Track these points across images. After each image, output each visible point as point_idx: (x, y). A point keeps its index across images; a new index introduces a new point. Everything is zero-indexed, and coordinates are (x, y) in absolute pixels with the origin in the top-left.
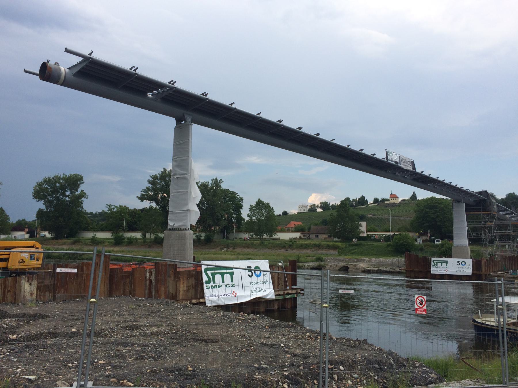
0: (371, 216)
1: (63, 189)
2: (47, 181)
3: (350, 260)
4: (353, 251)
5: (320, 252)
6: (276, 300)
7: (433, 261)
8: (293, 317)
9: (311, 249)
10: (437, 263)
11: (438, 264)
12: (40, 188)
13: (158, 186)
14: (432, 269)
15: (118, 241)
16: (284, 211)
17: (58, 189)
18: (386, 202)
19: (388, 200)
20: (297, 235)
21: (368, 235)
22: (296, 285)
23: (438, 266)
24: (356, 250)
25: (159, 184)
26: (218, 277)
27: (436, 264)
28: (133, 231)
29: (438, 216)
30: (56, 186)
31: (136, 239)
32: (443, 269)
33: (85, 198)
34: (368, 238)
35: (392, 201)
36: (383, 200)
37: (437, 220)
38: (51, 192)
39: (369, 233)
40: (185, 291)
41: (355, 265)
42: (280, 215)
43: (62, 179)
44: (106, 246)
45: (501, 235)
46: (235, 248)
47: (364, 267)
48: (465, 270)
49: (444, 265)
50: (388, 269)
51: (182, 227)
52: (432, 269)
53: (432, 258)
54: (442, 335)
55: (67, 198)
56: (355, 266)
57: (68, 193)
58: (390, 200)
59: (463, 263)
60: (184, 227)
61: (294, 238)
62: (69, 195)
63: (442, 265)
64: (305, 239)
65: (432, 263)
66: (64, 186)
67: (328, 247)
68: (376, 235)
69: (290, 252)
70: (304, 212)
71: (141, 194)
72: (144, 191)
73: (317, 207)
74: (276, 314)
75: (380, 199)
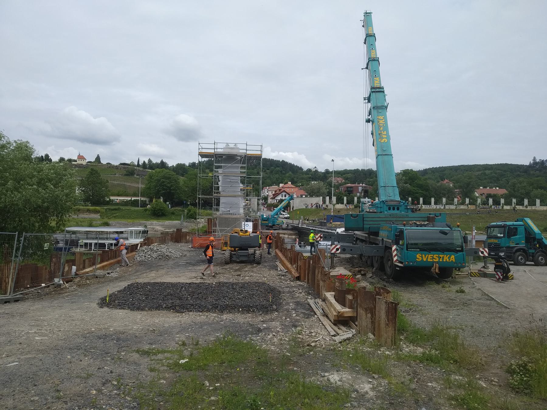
4: (115, 215)
18: (73, 163)
19: (75, 161)
24: (117, 214)
29: (172, 186)
35: (79, 162)
36: (70, 160)
54: (540, 212)
56: (154, 229)
58: (78, 161)
67: (89, 212)
68: (117, 199)
75: (66, 159)
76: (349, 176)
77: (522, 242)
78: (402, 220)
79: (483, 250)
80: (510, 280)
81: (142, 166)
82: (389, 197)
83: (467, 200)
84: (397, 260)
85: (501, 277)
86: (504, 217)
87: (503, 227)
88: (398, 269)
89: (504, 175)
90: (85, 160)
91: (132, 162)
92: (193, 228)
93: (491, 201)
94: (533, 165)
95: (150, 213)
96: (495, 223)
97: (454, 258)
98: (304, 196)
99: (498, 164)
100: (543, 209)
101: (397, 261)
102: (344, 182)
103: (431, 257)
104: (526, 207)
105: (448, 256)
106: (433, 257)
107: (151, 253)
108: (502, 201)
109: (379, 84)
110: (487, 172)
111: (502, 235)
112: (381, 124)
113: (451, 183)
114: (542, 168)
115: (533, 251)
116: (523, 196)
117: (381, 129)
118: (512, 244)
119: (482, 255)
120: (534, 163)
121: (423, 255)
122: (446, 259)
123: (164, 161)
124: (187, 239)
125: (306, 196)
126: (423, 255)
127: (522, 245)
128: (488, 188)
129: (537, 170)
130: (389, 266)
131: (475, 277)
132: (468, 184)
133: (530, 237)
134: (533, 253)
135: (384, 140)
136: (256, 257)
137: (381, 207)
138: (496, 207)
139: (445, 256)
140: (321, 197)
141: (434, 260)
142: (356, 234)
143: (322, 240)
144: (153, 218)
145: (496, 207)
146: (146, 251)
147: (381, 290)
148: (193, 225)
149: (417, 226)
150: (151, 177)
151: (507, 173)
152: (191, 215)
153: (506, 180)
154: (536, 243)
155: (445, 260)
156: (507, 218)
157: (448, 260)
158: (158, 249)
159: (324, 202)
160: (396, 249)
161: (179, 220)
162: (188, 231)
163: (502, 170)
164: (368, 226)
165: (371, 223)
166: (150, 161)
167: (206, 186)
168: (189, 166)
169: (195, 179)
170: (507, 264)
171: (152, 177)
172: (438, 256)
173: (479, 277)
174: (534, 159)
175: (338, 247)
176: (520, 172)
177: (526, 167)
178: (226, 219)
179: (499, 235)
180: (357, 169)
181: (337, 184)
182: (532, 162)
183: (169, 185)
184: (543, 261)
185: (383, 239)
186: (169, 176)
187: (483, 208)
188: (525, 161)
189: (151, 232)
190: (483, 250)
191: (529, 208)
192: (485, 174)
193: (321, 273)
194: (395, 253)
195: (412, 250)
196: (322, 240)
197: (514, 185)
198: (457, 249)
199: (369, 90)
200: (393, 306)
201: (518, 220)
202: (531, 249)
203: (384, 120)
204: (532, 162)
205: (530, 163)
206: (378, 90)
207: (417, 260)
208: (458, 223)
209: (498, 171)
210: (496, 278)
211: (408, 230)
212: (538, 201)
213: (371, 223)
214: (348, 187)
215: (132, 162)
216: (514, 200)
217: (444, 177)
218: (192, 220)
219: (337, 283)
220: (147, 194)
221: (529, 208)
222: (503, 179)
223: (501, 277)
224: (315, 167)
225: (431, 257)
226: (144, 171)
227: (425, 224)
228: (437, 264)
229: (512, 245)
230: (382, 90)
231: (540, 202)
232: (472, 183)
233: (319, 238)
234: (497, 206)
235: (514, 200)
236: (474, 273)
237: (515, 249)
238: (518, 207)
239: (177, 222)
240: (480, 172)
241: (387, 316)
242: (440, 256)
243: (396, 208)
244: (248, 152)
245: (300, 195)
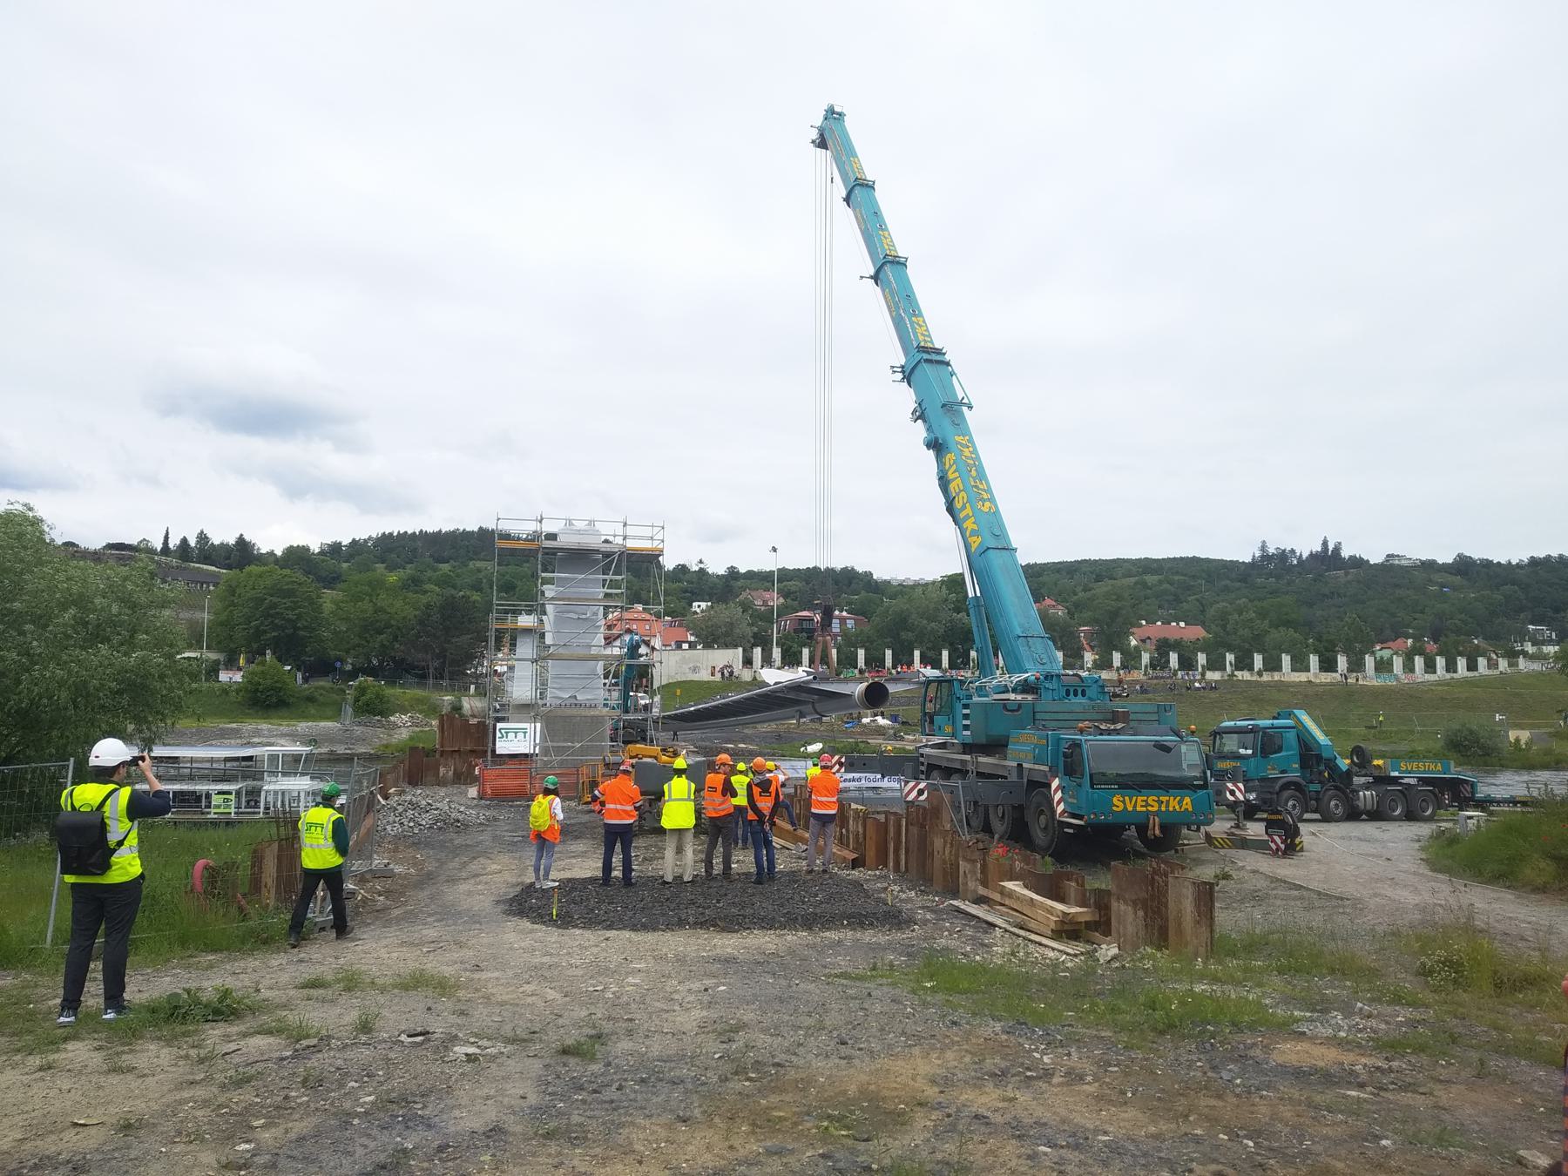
7: (500, 729)
11: (509, 734)
14: (498, 744)
23: (509, 738)
26: (313, 828)
27: (505, 735)
29: (299, 617)
32: (519, 744)
37: (299, 625)
40: (1470, 918)
45: (1261, 752)
49: (520, 735)
53: (498, 724)
63: (516, 737)
65: (498, 735)
76: (793, 585)
79: (1234, 788)
80: (1300, 854)
81: (175, 551)
83: (1117, 658)
84: (1064, 811)
85: (1283, 846)
86: (1208, 701)
87: (1251, 731)
88: (1071, 831)
89: (1193, 586)
91: (144, 539)
92: (385, 742)
93: (1174, 658)
94: (1260, 561)
95: (240, 699)
96: (1232, 723)
97: (1190, 803)
98: (685, 646)
99: (1175, 558)
100: (1297, 680)
101: (1066, 815)
102: (783, 604)
103: (1142, 801)
104: (1260, 674)
105: (1178, 798)
106: (1146, 801)
107: (413, 814)
108: (1202, 659)
110: (1151, 579)
111: (1250, 752)
113: (1060, 607)
114: (1282, 569)
115: (1315, 787)
116: (1247, 646)
118: (1273, 772)
119: (1231, 798)
120: (1262, 557)
121: (1127, 798)
122: (1174, 804)
123: (247, 538)
124: (441, 774)
125: (692, 646)
126: (1127, 798)
127: (1294, 775)
128: (1159, 623)
129: (1270, 575)
130: (1043, 826)
131: (1223, 848)
132: (1114, 614)
133: (1309, 755)
134: (1318, 792)
136: (703, 816)
137: (1052, 690)
138: (1188, 674)
139: (1172, 798)
140: (740, 649)
141: (1150, 808)
142: (928, 756)
143: (843, 770)
145: (1188, 674)
146: (400, 809)
147: (1162, 866)
148: (382, 733)
149: (1101, 734)
150: (232, 591)
151: (1200, 581)
152: (368, 705)
153: (1197, 600)
154: (1322, 768)
155: (1171, 809)
156: (1216, 702)
157: (1177, 807)
158: (429, 804)
159: (748, 662)
160: (1060, 787)
161: (336, 715)
162: (372, 752)
163: (1185, 575)
166: (202, 538)
167: (404, 618)
168: (322, 553)
169: (371, 595)
170: (1292, 817)
171: (238, 591)
172: (1157, 799)
173: (1230, 848)
174: (1263, 547)
175: (922, 786)
176: (1232, 581)
177: (1243, 568)
178: (565, 718)
179: (1242, 751)
180: (815, 568)
181: (763, 608)
182: (1258, 554)
183: (291, 615)
184: (1340, 811)
185: (1020, 766)
186: (290, 586)
187: (1156, 678)
188: (1244, 554)
190: (1234, 788)
191: (1266, 677)
192: (1145, 585)
193: (951, 844)
194: (1059, 795)
195: (1103, 787)
196: (843, 770)
197: (1223, 617)
198: (1195, 783)
200: (1206, 889)
201: (1279, 714)
202: (1312, 782)
204: (1257, 555)
205: (1254, 556)
207: (1114, 808)
208: (1193, 727)
209: (1176, 578)
210: (1271, 849)
211: (1091, 743)
212: (1286, 660)
214: (802, 620)
215: (144, 539)
216: (1230, 657)
217: (1042, 591)
218: (376, 718)
219: (1017, 862)
220: (219, 643)
221: (1266, 677)
222: (1190, 599)
223: (1283, 846)
224: (701, 562)
225: (1142, 801)
226: (185, 569)
227: (1118, 728)
228: (1156, 818)
229: (1274, 774)
231: (1291, 660)
232: (1124, 612)
233: (837, 767)
234: (1190, 673)
235: (1230, 657)
236: (1220, 840)
237: (1280, 783)
238: (1239, 674)
239: (330, 724)
240: (1133, 580)
241: (1198, 907)
242: (1161, 798)
243: (1080, 692)
244: (631, 544)
245: (673, 643)
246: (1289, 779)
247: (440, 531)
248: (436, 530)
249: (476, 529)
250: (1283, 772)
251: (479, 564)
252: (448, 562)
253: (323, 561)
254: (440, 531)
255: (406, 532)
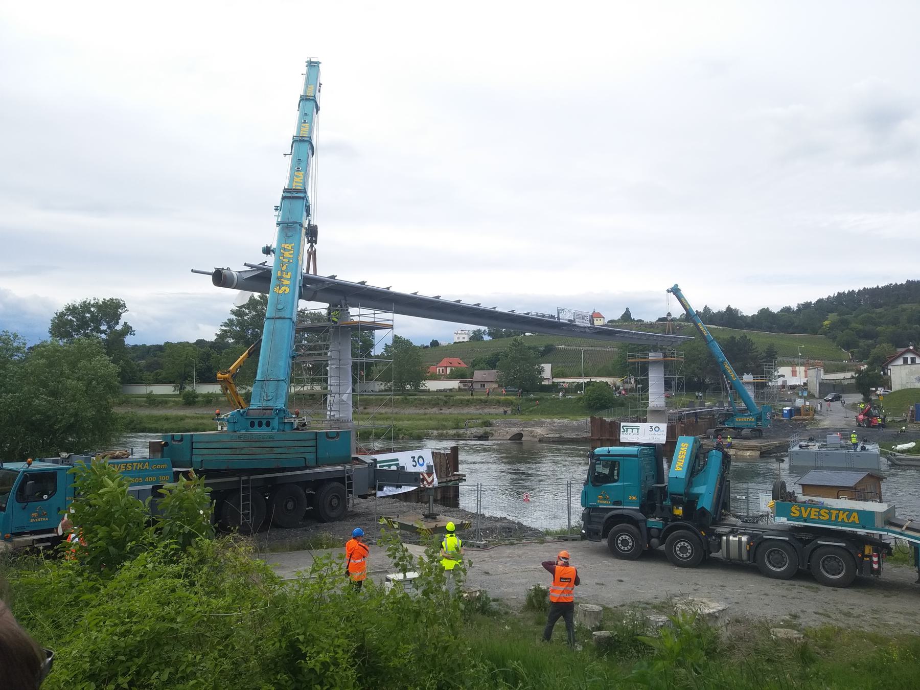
0: (563, 346)
1: (96, 320)
2: (72, 310)
3: (525, 424)
5: (486, 411)
6: (439, 488)
7: (623, 427)
8: (456, 505)
9: (475, 406)
10: (627, 429)
12: (60, 321)
13: (246, 318)
14: (622, 436)
15: (190, 401)
16: (433, 341)
17: (88, 321)
20: (454, 384)
21: (553, 382)
22: (458, 471)
23: (628, 433)
25: (247, 314)
28: (206, 383)
30: (84, 317)
31: (217, 396)
32: (634, 436)
33: (131, 334)
34: (554, 388)
38: (78, 325)
39: (556, 380)
41: (531, 432)
42: (427, 347)
43: (93, 306)
44: (170, 408)
46: (367, 407)
47: (542, 433)
48: (658, 437)
49: (635, 431)
50: (573, 436)
51: (344, 419)
52: (621, 437)
55: (103, 336)
57: (104, 327)
59: (657, 429)
60: (346, 419)
61: (450, 390)
62: (106, 331)
64: (465, 390)
65: (622, 430)
66: (97, 316)
68: (564, 382)
69: (446, 411)
70: (463, 342)
71: (221, 330)
72: (226, 325)
73: (484, 333)
74: (439, 502)
77: (631, 498)
78: (262, 446)
82: (265, 403)
90: (602, 319)
103: (815, 512)
109: (301, 183)
112: (287, 258)
117: (284, 268)
121: (803, 509)
123: (733, 307)
126: (803, 509)
135: (283, 289)
144: (586, 413)
164: (199, 459)
165: (205, 452)
189: (529, 438)
199: (309, 193)
203: (292, 252)
206: (295, 195)
213: (205, 452)
225: (815, 512)
229: (604, 504)
230: (302, 195)
243: (264, 423)
246: (625, 512)
247: (878, 287)
248: (875, 286)
249: (904, 282)
250: (615, 503)
251: (905, 306)
252: (881, 307)
253: (783, 315)
254: (878, 287)
255: (896, 284)
